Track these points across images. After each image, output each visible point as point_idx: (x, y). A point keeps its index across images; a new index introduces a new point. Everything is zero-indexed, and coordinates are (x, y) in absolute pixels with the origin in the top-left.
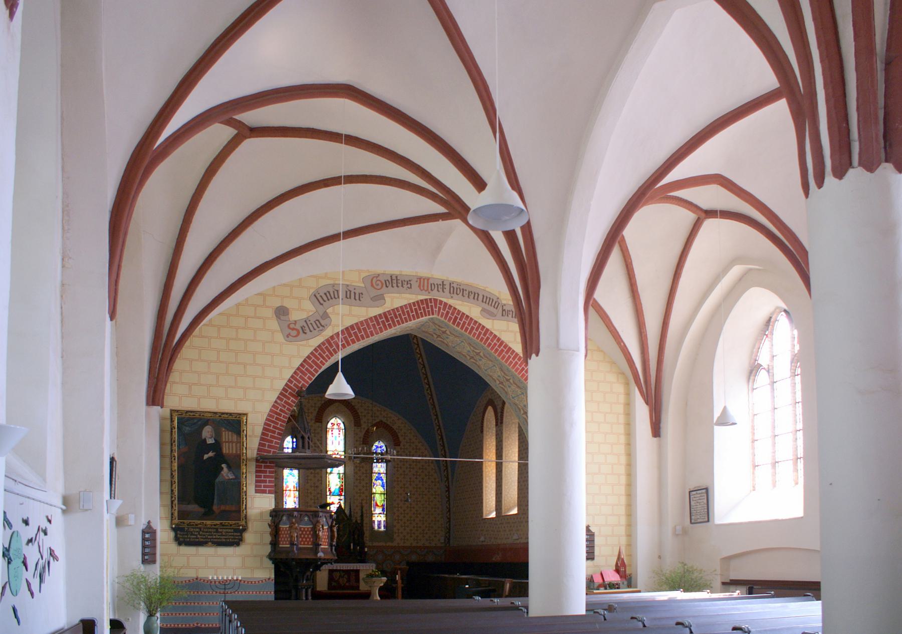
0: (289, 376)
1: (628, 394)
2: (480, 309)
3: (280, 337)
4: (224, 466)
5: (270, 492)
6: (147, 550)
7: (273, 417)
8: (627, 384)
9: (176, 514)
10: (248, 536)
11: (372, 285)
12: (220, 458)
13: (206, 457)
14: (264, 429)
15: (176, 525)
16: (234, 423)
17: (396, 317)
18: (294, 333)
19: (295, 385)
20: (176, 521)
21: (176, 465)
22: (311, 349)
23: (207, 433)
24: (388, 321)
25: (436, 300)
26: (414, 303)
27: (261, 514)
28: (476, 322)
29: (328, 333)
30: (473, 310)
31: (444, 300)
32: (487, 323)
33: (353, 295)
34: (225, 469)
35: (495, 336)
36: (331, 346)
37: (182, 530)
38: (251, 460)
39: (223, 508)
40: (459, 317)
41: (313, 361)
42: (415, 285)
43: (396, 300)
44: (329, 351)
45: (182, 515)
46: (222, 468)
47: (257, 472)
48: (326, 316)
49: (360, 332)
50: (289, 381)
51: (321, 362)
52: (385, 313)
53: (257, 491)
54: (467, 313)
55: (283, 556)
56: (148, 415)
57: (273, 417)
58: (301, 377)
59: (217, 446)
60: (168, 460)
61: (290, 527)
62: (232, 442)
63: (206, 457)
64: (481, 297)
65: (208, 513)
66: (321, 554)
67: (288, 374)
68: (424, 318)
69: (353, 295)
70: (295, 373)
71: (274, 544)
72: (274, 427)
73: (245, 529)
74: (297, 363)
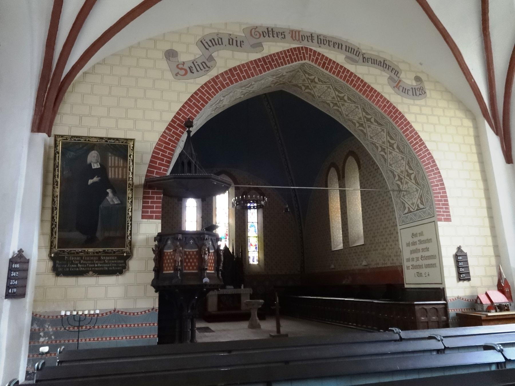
0: (177, 109)
1: (477, 128)
2: (344, 56)
3: (169, 75)
4: (108, 191)
5: (157, 218)
6: (13, 282)
7: (162, 146)
8: (474, 120)
9: (56, 242)
10: (133, 264)
11: (251, 35)
12: (106, 183)
13: (90, 182)
14: (153, 157)
15: (56, 254)
16: (121, 148)
17: (273, 61)
18: (182, 72)
19: (183, 117)
20: (56, 250)
21: (58, 190)
22: (198, 87)
23: (93, 159)
24: (266, 64)
25: (306, 49)
26: (288, 50)
27: (147, 240)
28: (342, 67)
29: (214, 73)
30: (338, 57)
31: (314, 48)
32: (351, 68)
33: (234, 42)
34: (110, 194)
35: (359, 78)
36: (217, 84)
37: (62, 259)
38: (137, 187)
39: (107, 234)
40: (327, 63)
41: (200, 97)
42: (288, 36)
43: (272, 47)
44: (214, 88)
45: (63, 243)
46: (108, 193)
47: (144, 198)
48: (211, 58)
49: (242, 73)
50: (178, 113)
51: (208, 98)
52: (263, 58)
53: (143, 217)
54: (334, 59)
55: (166, 283)
56: (31, 143)
57: (162, 146)
58: (188, 110)
59: (103, 171)
60: (50, 188)
61: (175, 251)
62: (118, 167)
63: (90, 182)
64: (344, 47)
65: (91, 242)
66: (206, 280)
67: (177, 107)
68: (298, 62)
69: (234, 42)
70: (183, 106)
71: (158, 270)
72: (162, 155)
73: (129, 256)
74: (185, 98)
